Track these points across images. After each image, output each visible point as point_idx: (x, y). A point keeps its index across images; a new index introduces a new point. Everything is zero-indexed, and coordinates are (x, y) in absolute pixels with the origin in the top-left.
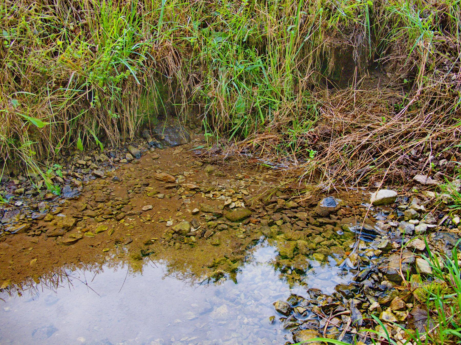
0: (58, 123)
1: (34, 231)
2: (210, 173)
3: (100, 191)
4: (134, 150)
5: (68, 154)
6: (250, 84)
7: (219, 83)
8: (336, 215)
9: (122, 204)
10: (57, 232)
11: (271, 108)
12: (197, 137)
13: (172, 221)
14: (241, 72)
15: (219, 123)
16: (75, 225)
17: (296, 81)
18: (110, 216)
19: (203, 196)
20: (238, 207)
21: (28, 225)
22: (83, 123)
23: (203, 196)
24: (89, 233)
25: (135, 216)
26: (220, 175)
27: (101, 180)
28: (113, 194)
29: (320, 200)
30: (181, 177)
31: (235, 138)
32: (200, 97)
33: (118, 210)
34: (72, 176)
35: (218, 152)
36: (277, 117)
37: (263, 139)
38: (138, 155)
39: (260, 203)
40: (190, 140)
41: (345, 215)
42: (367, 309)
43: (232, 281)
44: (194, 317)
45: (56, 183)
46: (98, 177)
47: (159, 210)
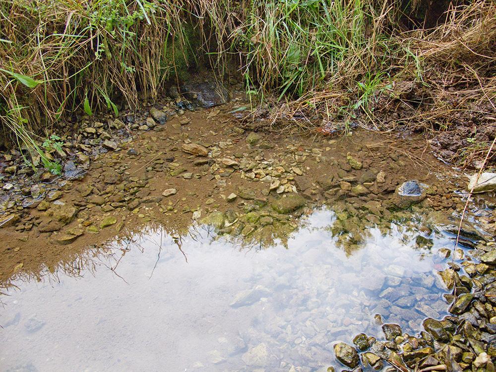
0: (55, 81)
1: (24, 225)
2: (253, 143)
3: (111, 168)
4: (157, 114)
5: (74, 120)
6: (307, 25)
7: (266, 24)
8: (421, 207)
9: (138, 187)
10: (53, 225)
11: (334, 57)
12: (237, 96)
13: (200, 212)
14: (295, 7)
15: (265, 77)
16: (76, 216)
17: (368, 21)
18: (121, 204)
19: (242, 176)
20: (288, 192)
21: (17, 215)
22: (90, 80)
23: (242, 176)
24: (92, 228)
25: (153, 203)
26: (266, 146)
27: (114, 154)
28: (127, 173)
29: (398, 184)
30: (215, 149)
31: (287, 96)
32: (241, 43)
33: (132, 194)
34: (78, 149)
35: (265, 115)
36: (342, 69)
37: (324, 98)
38: (163, 120)
39: (318, 187)
40: (229, 100)
41: (433, 207)
42: (471, 364)
43: (282, 247)
44: (220, 359)
45: (58, 158)
46: (110, 149)
47: (185, 195)
